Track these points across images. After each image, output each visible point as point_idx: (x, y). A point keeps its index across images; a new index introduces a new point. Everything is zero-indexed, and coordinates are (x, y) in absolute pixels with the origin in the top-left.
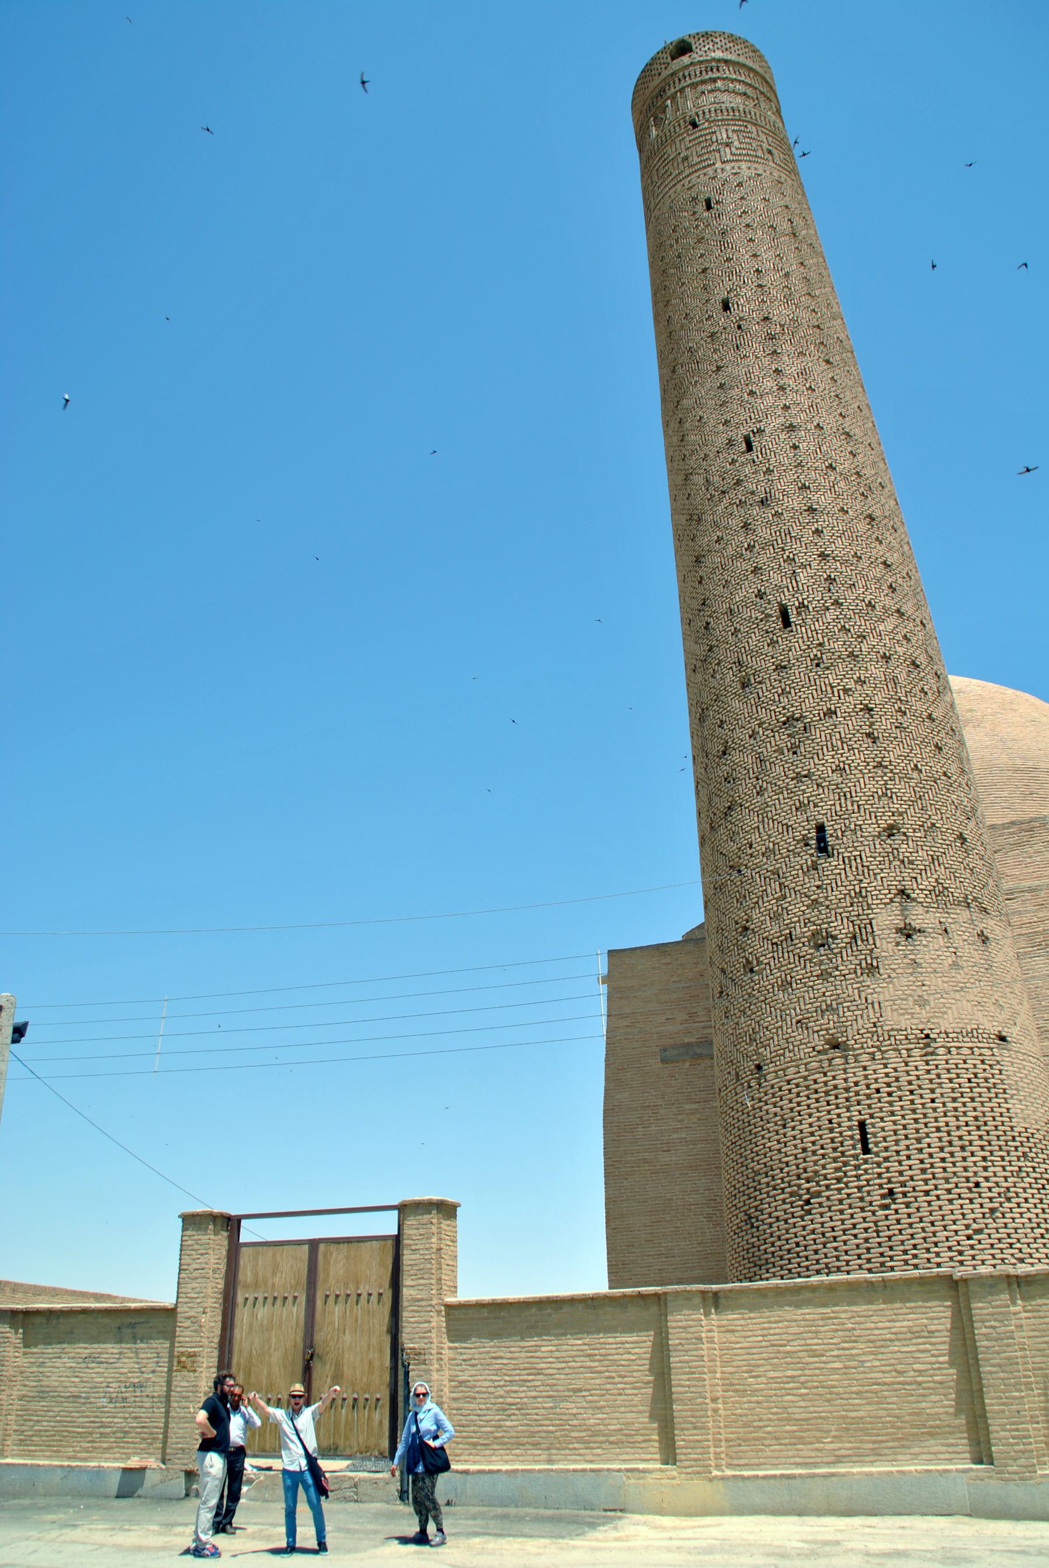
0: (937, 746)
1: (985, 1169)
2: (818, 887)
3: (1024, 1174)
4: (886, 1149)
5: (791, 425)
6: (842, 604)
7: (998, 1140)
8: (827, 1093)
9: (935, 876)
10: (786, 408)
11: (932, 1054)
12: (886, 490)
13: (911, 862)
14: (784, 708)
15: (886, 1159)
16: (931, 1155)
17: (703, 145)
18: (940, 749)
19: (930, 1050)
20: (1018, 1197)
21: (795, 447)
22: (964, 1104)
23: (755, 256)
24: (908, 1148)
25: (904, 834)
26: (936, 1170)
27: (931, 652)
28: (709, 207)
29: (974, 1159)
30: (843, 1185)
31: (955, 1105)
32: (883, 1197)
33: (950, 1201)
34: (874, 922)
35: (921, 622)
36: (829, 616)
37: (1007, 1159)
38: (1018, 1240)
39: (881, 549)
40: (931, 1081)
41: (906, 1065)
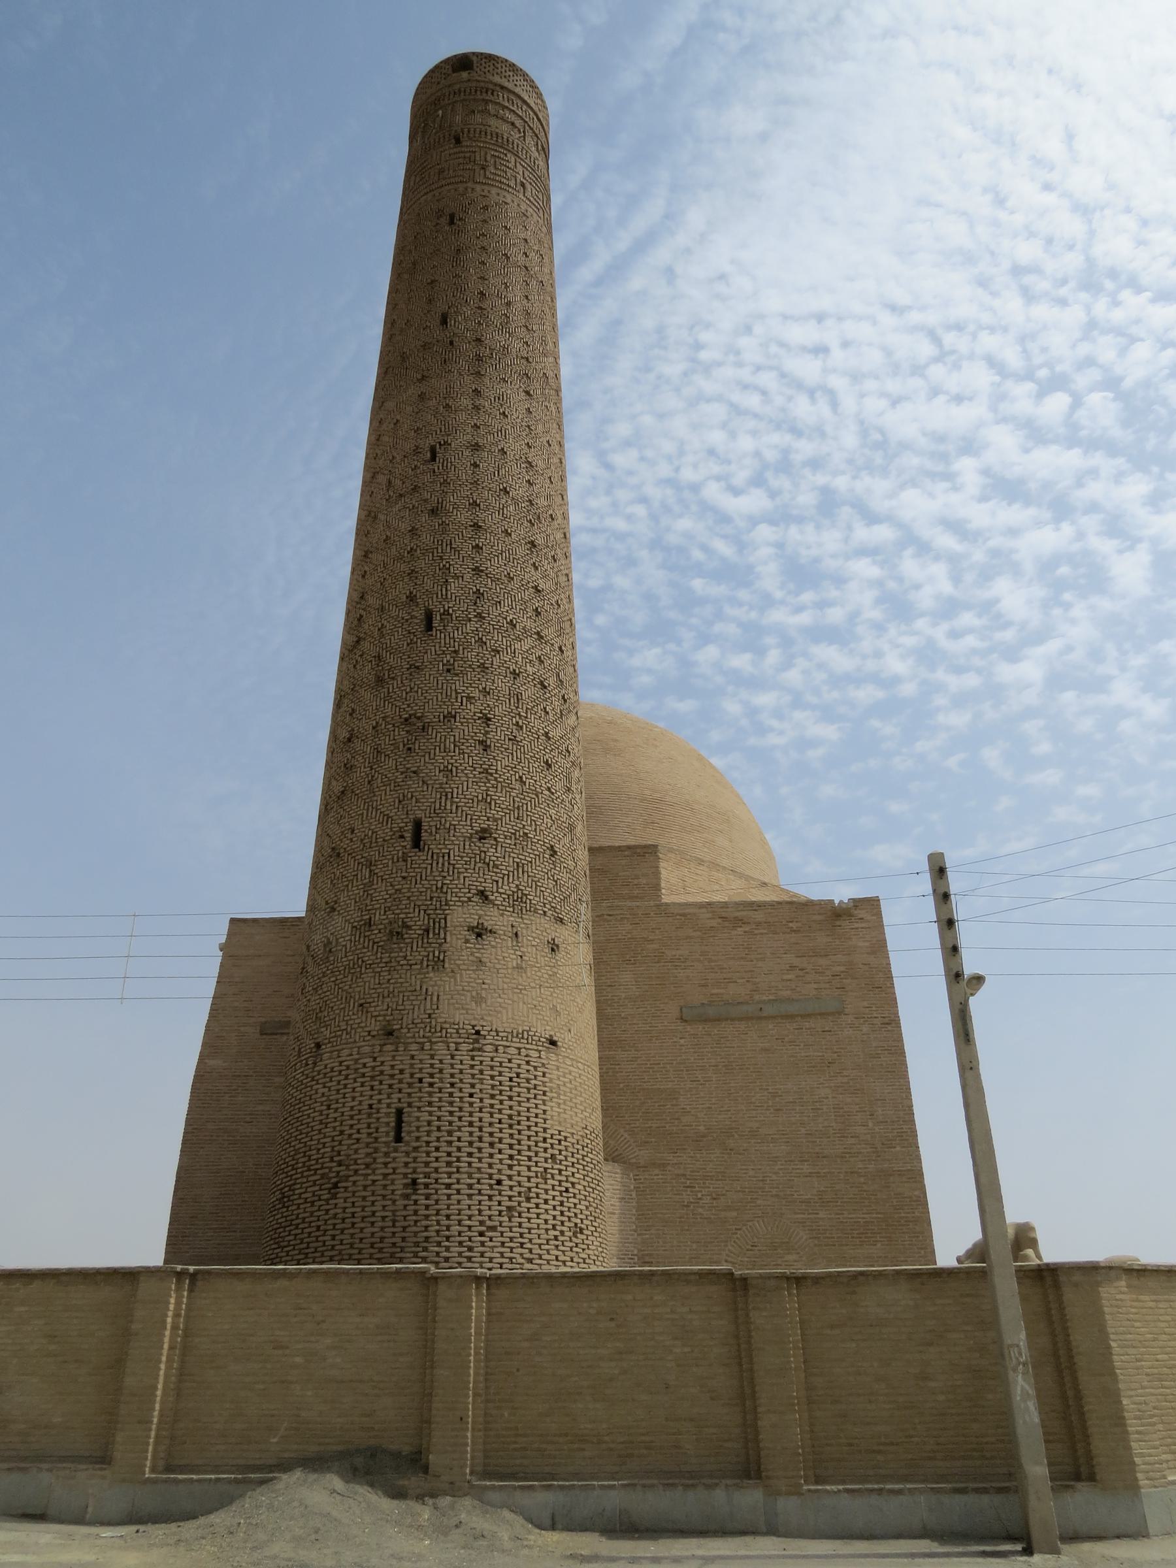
0: (547, 763)
1: (510, 1167)
2: (404, 878)
3: (549, 1176)
4: (418, 1139)
5: (477, 444)
6: (484, 618)
7: (529, 1139)
8: (373, 1078)
9: (517, 882)
10: (476, 427)
11: (480, 1050)
12: (555, 523)
13: (495, 866)
14: (409, 706)
15: (416, 1149)
16: (459, 1149)
17: (461, 160)
18: (550, 766)
20: (538, 1197)
21: (476, 465)
22: (501, 1102)
23: (483, 278)
24: (438, 1139)
25: (495, 839)
26: (462, 1165)
27: (562, 676)
28: (452, 222)
29: (500, 1156)
30: (370, 1171)
31: (493, 1102)
33: (470, 1196)
34: (449, 917)
35: (560, 648)
36: (470, 627)
37: (534, 1159)
38: (530, 1240)
39: (536, 575)
40: (473, 1076)
41: (452, 1058)
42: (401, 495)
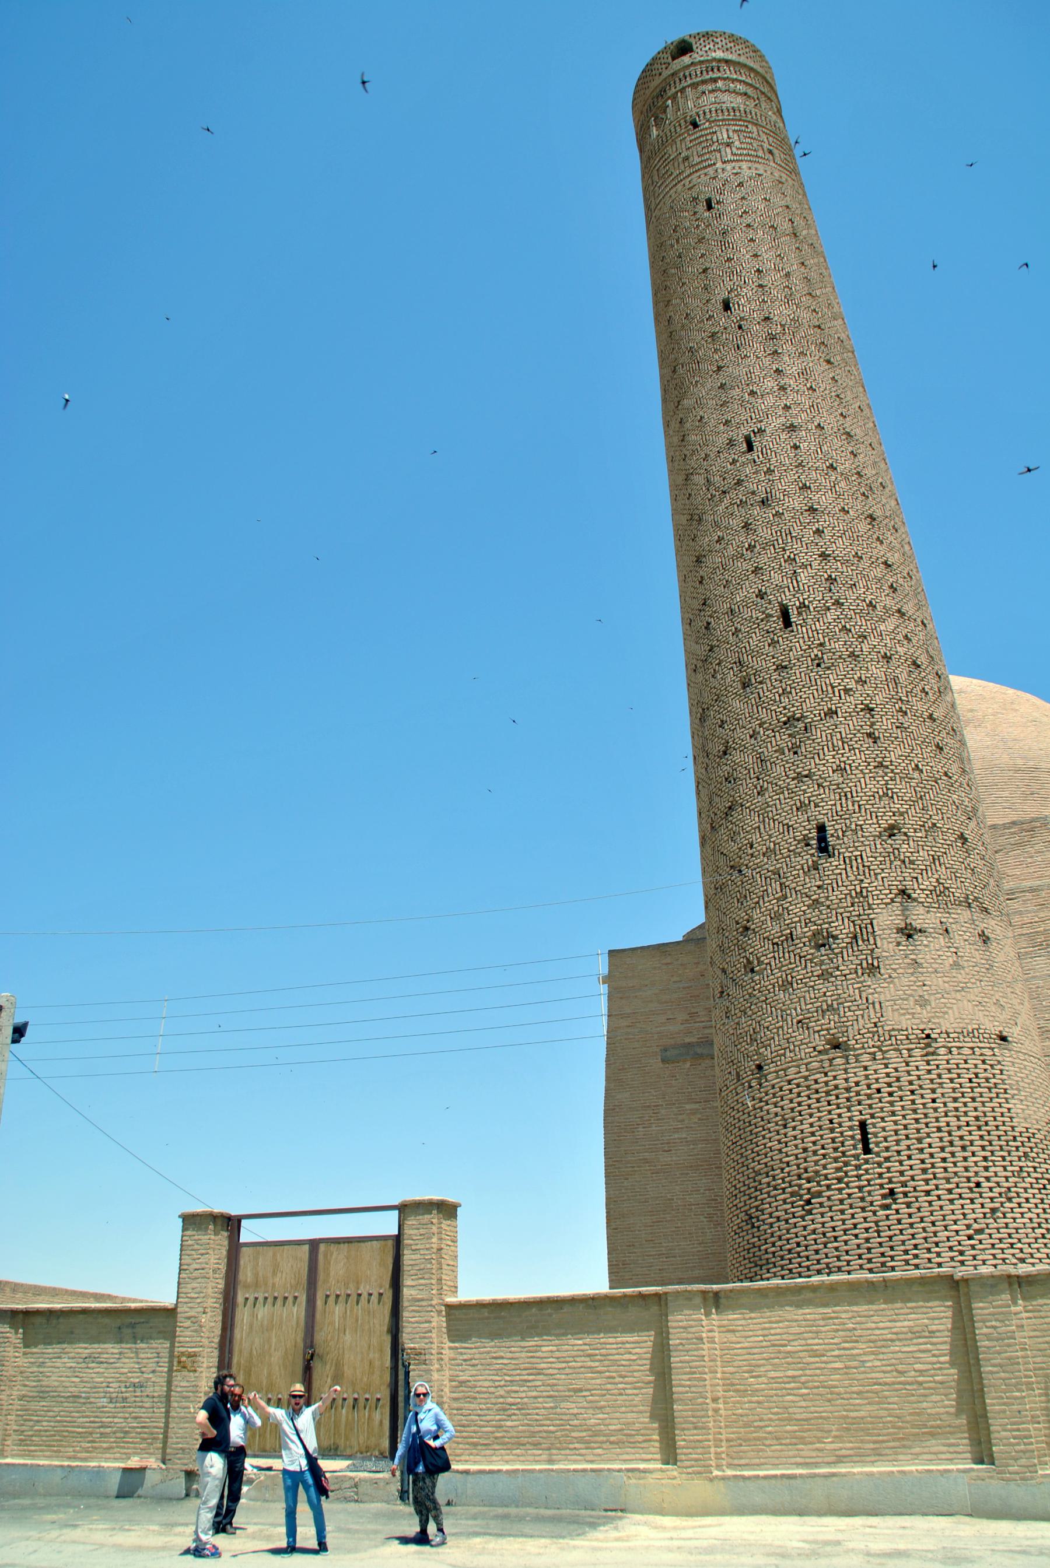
0: (937, 746)
1: (986, 1169)
2: (819, 887)
3: (1025, 1174)
4: (887, 1149)
5: (792, 425)
6: (842, 604)
7: (999, 1140)
8: (828, 1093)
9: (936, 876)
10: (787, 408)
11: (933, 1054)
12: (887, 490)
13: (912, 862)
14: (785, 708)
15: (887, 1159)
16: (932, 1155)
17: (703, 145)
18: (941, 749)
19: (931, 1050)
20: (1019, 1197)
21: (796, 447)
22: (965, 1104)
23: (756, 256)
24: (909, 1148)
25: (905, 834)
26: (937, 1170)
27: (932, 652)
28: (709, 207)
29: (975, 1159)
30: (843, 1185)
31: (956, 1105)
32: (884, 1197)
33: (951, 1201)
34: (874, 922)
35: (922, 622)
36: (830, 616)
37: (1008, 1159)
38: (1019, 1240)
39: (882, 549)
40: (932, 1081)
41: (907, 1065)
42: (724, 492)
